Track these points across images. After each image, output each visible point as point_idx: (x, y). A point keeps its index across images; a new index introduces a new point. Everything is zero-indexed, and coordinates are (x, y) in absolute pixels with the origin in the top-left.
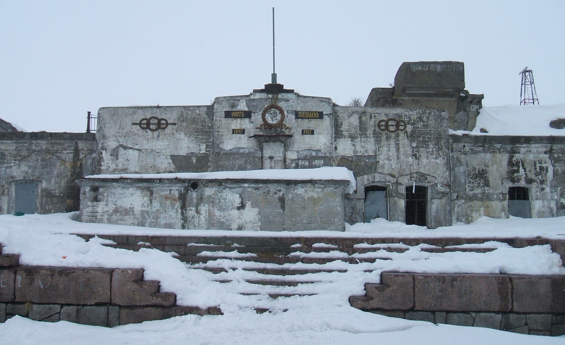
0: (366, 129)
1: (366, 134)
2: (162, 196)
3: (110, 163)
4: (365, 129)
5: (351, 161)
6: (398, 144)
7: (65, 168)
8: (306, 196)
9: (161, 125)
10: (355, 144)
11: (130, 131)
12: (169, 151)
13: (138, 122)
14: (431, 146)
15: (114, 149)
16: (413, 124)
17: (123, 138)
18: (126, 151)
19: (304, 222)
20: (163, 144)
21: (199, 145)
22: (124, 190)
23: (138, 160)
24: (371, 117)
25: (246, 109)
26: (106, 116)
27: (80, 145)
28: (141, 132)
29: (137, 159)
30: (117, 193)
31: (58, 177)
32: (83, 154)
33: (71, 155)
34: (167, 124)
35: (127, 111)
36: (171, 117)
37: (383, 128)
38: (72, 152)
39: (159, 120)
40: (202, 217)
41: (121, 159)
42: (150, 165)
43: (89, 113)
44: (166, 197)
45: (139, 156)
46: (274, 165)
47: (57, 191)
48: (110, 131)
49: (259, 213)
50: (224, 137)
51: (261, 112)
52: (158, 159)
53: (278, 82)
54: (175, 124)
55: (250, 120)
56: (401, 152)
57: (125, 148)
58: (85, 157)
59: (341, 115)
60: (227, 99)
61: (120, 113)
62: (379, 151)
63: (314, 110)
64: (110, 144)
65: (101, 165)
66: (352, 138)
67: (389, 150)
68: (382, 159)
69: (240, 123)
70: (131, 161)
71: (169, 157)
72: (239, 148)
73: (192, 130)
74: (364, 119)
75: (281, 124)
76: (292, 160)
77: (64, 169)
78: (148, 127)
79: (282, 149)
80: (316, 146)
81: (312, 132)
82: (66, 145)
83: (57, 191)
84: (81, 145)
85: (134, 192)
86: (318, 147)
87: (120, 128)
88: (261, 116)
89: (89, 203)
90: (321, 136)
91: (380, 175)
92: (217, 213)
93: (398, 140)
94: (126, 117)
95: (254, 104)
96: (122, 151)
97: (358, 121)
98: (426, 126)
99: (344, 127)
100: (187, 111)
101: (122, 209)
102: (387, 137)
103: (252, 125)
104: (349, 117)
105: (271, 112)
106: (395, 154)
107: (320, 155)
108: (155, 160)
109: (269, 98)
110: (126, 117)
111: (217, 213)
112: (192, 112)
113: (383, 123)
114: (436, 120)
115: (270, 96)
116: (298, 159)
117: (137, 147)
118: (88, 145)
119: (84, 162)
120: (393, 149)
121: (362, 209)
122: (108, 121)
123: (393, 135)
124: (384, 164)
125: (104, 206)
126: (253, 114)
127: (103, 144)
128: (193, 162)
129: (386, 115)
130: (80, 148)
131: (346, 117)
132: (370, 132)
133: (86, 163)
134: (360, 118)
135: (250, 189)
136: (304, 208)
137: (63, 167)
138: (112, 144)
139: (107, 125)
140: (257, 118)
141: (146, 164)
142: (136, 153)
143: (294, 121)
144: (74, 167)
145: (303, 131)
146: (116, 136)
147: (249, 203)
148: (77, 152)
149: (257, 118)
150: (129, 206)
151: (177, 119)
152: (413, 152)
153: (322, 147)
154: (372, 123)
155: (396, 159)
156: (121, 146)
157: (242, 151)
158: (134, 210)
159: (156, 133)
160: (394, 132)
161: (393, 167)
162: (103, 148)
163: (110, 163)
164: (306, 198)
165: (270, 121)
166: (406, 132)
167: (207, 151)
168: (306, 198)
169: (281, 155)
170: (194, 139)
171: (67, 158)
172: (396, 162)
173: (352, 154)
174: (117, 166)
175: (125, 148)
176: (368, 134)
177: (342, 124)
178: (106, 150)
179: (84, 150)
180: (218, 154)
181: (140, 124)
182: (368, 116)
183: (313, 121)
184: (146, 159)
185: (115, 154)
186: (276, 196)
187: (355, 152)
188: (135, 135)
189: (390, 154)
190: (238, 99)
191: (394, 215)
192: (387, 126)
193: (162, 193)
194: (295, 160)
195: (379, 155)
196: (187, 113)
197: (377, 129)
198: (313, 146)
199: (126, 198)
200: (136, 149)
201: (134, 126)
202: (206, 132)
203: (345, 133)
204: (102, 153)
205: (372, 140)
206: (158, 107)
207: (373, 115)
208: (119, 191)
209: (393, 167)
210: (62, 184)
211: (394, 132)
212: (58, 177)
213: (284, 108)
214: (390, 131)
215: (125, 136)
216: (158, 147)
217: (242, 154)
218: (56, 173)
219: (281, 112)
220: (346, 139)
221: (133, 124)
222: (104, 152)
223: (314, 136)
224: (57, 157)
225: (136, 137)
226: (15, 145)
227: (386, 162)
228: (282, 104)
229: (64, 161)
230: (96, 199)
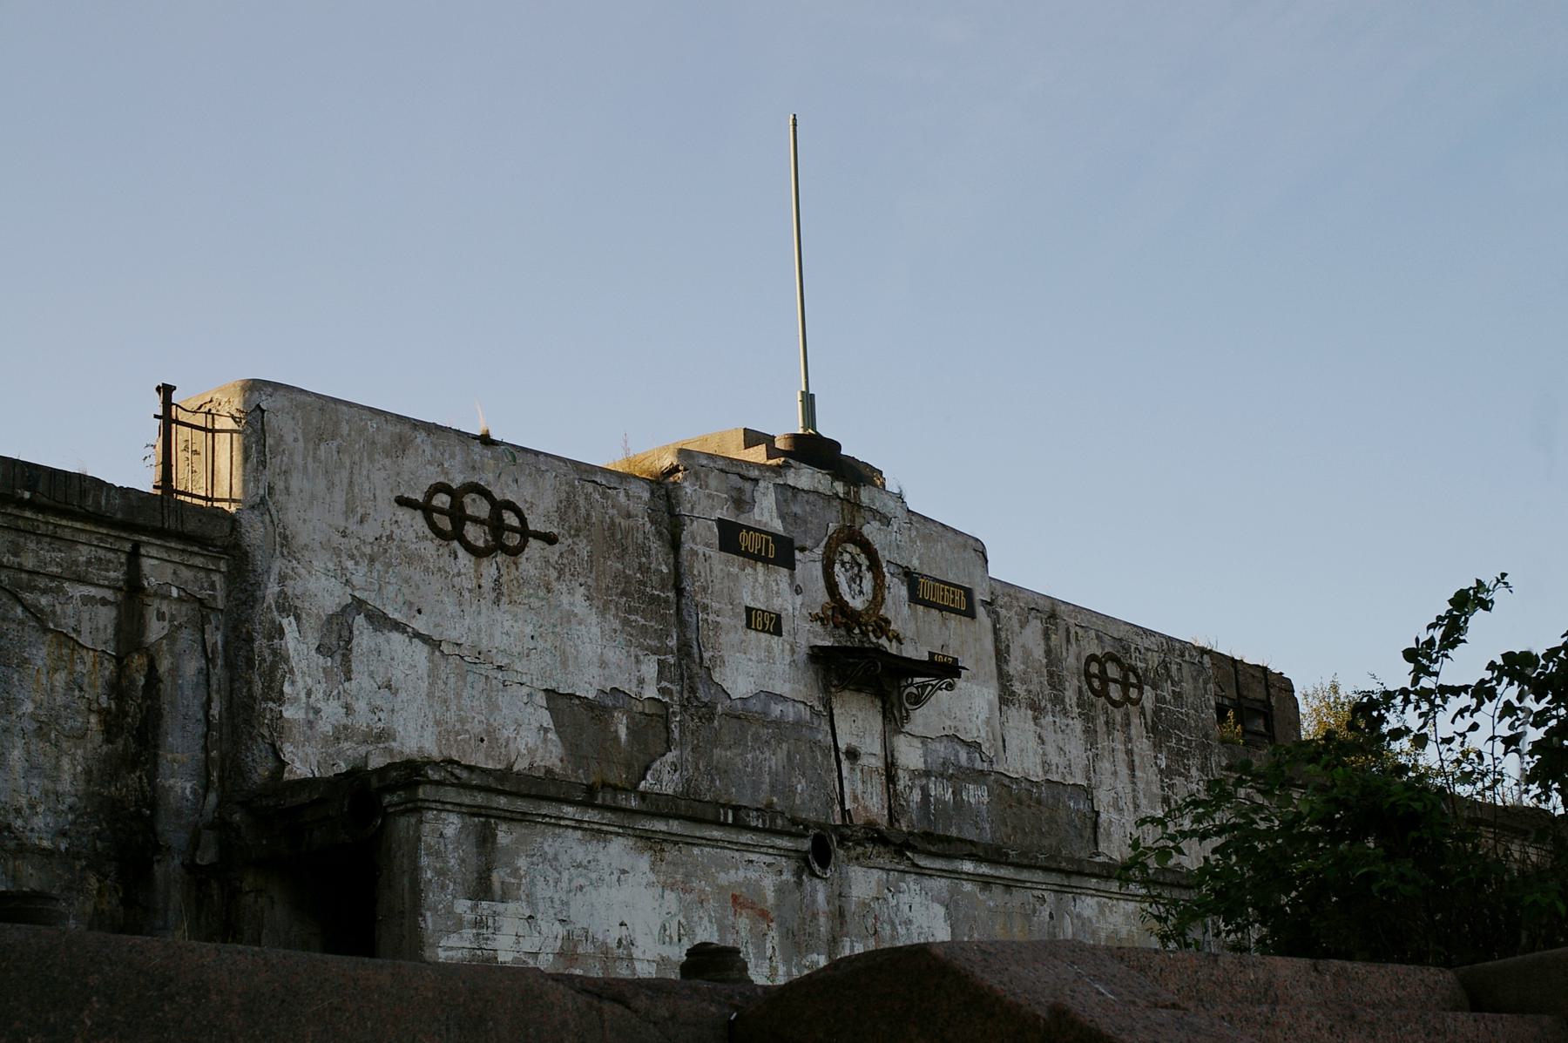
2: (721, 888)
3: (318, 694)
7: (74, 684)
9: (504, 534)
11: (390, 538)
12: (536, 671)
13: (420, 498)
14: (1194, 772)
15: (331, 618)
16: (1155, 687)
17: (363, 568)
18: (380, 638)
20: (517, 627)
21: (638, 661)
22: (594, 847)
23: (430, 695)
25: (777, 526)
26: (284, 425)
27: (147, 564)
28: (430, 548)
29: (424, 686)
30: (565, 859)
31: (41, 732)
32: (161, 616)
33: (106, 616)
35: (372, 426)
36: (539, 505)
38: (109, 595)
39: (499, 506)
41: (361, 681)
42: (477, 729)
43: (166, 391)
44: (735, 898)
45: (433, 674)
47: (38, 822)
48: (310, 515)
51: (819, 551)
52: (502, 700)
53: (825, 429)
54: (550, 539)
55: (792, 576)
56: (1141, 786)
57: (380, 621)
58: (170, 637)
60: (721, 464)
61: (345, 429)
63: (951, 578)
64: (312, 585)
65: (280, 698)
69: (766, 585)
70: (402, 695)
71: (541, 699)
73: (608, 580)
76: (914, 774)
77: (69, 689)
79: (877, 723)
82: (83, 553)
83: (38, 822)
84: (156, 568)
85: (626, 862)
87: (349, 510)
88: (819, 565)
89: (462, 906)
93: (1130, 740)
94: (371, 460)
98: (1177, 696)
100: (590, 488)
101: (590, 949)
103: (799, 599)
106: (1129, 789)
108: (493, 706)
110: (371, 460)
112: (604, 495)
114: (1195, 680)
116: (927, 774)
117: (419, 624)
118: (186, 574)
119: (164, 665)
122: (298, 459)
125: (522, 928)
126: (798, 555)
127: (282, 579)
128: (617, 738)
130: (151, 582)
132: (1070, 696)
133: (175, 670)
137: (60, 678)
138: (322, 591)
139: (295, 483)
141: (462, 721)
142: (421, 651)
143: (905, 610)
144: (117, 688)
146: (337, 552)
148: (133, 592)
150: (616, 933)
151: (555, 517)
152: (1163, 789)
156: (359, 605)
158: (637, 953)
159: (489, 569)
162: (286, 606)
163: (318, 694)
166: (1143, 713)
167: (662, 691)
169: (877, 748)
170: (617, 625)
171: (85, 627)
174: (348, 709)
175: (380, 621)
178: (298, 618)
179: (167, 597)
180: (710, 707)
181: (427, 509)
184: (459, 696)
185: (337, 641)
188: (411, 558)
190: (755, 473)
193: (723, 878)
196: (588, 497)
199: (603, 890)
200: (417, 635)
201: (404, 515)
202: (654, 600)
204: (281, 633)
206: (485, 440)
208: (572, 847)
210: (65, 785)
212: (41, 732)
213: (884, 555)
215: (372, 560)
216: (500, 641)
218: (28, 707)
221: (403, 502)
222: (288, 624)
224: (35, 613)
225: (416, 574)
229: (67, 641)
230: (482, 889)
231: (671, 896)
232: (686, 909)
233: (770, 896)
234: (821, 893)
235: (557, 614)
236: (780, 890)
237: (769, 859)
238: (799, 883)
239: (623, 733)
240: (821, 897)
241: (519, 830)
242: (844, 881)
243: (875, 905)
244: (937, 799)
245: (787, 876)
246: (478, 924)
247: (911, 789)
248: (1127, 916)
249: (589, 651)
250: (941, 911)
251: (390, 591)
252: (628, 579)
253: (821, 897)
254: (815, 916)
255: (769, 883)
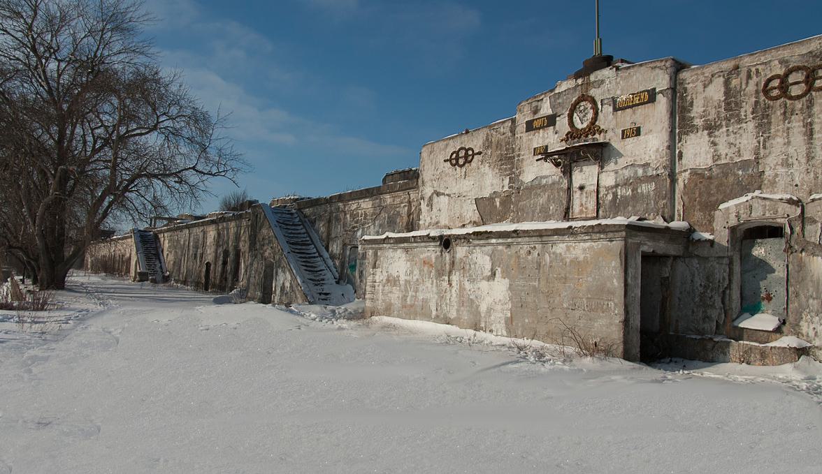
0: (738, 105)
1: (738, 115)
4: (736, 104)
5: (710, 178)
6: (811, 124)
8: (569, 257)
10: (717, 140)
19: (565, 306)
24: (749, 77)
34: (473, 155)
37: (775, 93)
39: (467, 150)
40: (453, 291)
46: (585, 199)
49: (511, 288)
50: (525, 163)
55: (554, 128)
57: (438, 194)
59: (691, 85)
62: (765, 148)
66: (711, 128)
67: (789, 143)
68: (771, 165)
72: (542, 177)
74: (734, 82)
75: (593, 128)
76: (608, 189)
78: (457, 163)
80: (643, 156)
81: (637, 132)
86: (646, 159)
90: (650, 136)
91: (763, 203)
92: (467, 285)
95: (560, 101)
96: (435, 199)
97: (723, 90)
99: (697, 110)
102: (785, 113)
104: (705, 86)
105: (582, 108)
106: (803, 150)
107: (651, 172)
108: (462, 207)
109: (578, 85)
111: (467, 285)
113: (776, 83)
115: (580, 81)
116: (617, 186)
117: (447, 192)
120: (798, 138)
121: (724, 279)
123: (798, 104)
124: (777, 175)
129: (782, 62)
131: (700, 88)
132: (747, 108)
134: (727, 83)
135: (500, 248)
136: (565, 280)
140: (563, 124)
145: (623, 131)
147: (499, 269)
149: (563, 124)
153: (653, 157)
154: (751, 88)
155: (803, 161)
156: (435, 192)
157: (544, 181)
160: (798, 97)
161: (797, 181)
164: (568, 260)
165: (579, 126)
168: (568, 260)
172: (803, 167)
173: (710, 162)
176: (743, 114)
177: (692, 104)
181: (450, 160)
182: (743, 75)
183: (640, 110)
186: (530, 257)
187: (716, 157)
189: (791, 150)
191: (797, 295)
192: (784, 88)
194: (612, 188)
195: (765, 157)
197: (762, 98)
198: (638, 159)
203: (698, 122)
205: (751, 126)
207: (753, 69)
209: (797, 181)
211: (798, 97)
214: (791, 98)
216: (465, 189)
217: (544, 186)
219: (593, 102)
220: (700, 132)
221: (445, 161)
223: (641, 137)
226: (371, 202)
227: (781, 170)
228: (593, 92)
231: (409, 263)
232: (412, 266)
233: (434, 260)
234: (447, 256)
235: (480, 175)
236: (436, 258)
237: (433, 249)
238: (442, 255)
239: (498, 204)
240: (448, 258)
241: (381, 251)
242: (455, 252)
243: (464, 259)
244: (621, 197)
245: (439, 253)
246: (373, 274)
247: (606, 195)
248: (584, 250)
249: (488, 182)
250: (489, 258)
251: (441, 185)
252: (502, 155)
253: (448, 258)
254: (445, 265)
255: (433, 256)
